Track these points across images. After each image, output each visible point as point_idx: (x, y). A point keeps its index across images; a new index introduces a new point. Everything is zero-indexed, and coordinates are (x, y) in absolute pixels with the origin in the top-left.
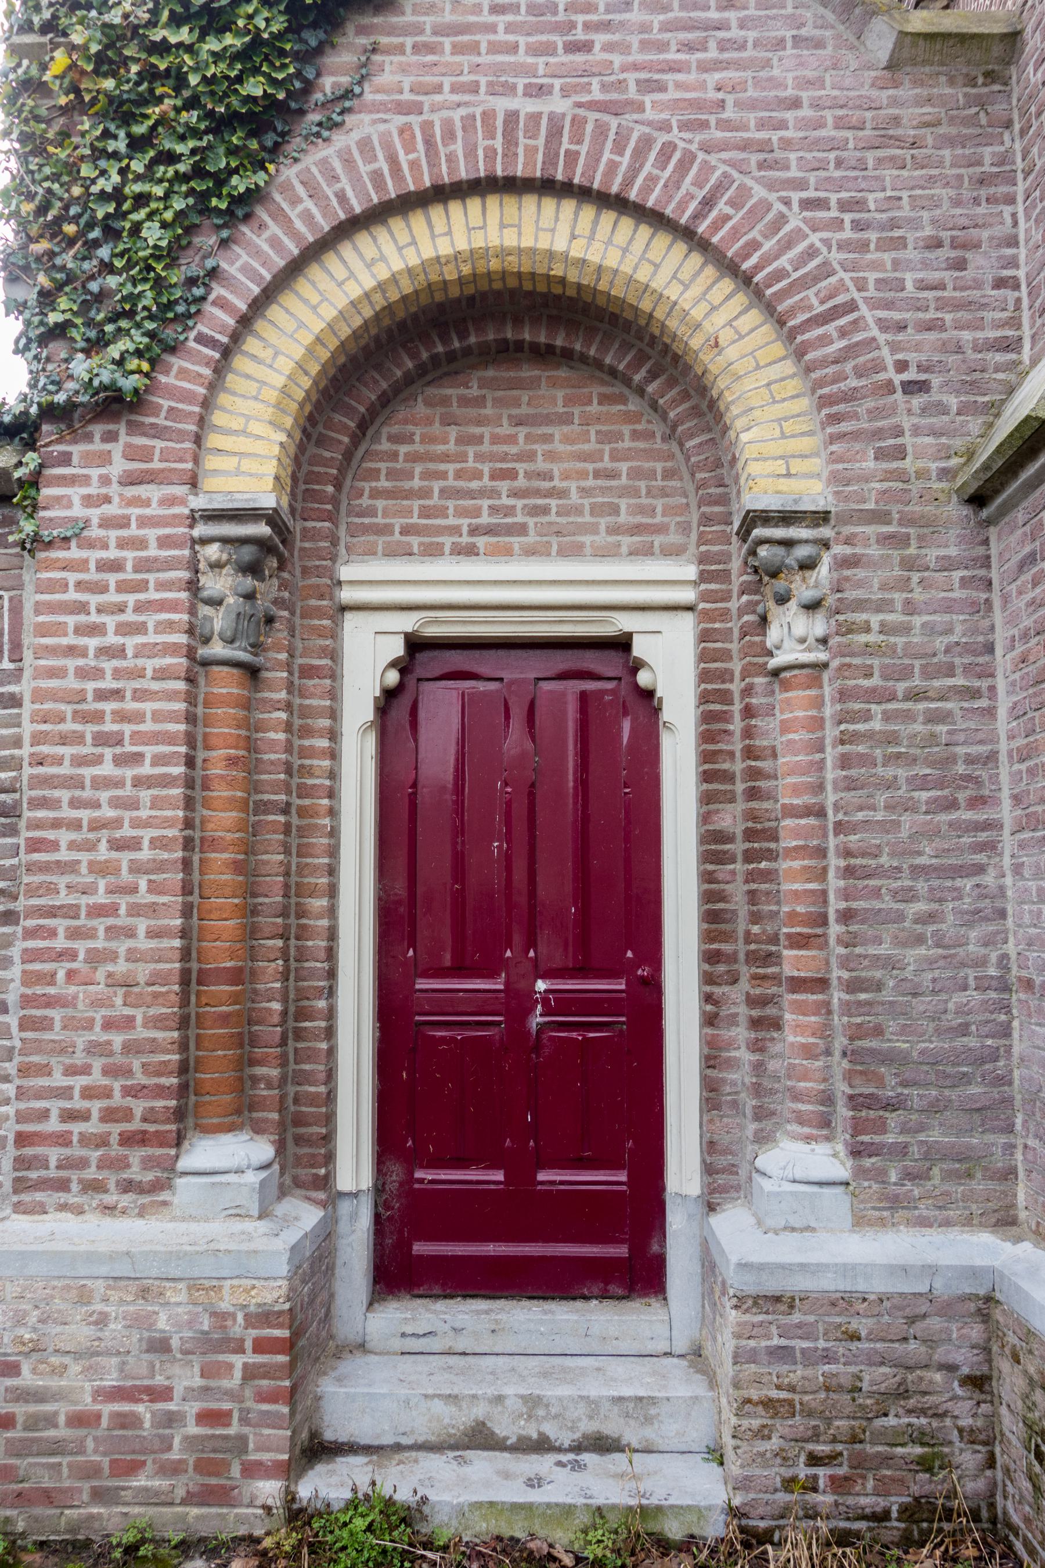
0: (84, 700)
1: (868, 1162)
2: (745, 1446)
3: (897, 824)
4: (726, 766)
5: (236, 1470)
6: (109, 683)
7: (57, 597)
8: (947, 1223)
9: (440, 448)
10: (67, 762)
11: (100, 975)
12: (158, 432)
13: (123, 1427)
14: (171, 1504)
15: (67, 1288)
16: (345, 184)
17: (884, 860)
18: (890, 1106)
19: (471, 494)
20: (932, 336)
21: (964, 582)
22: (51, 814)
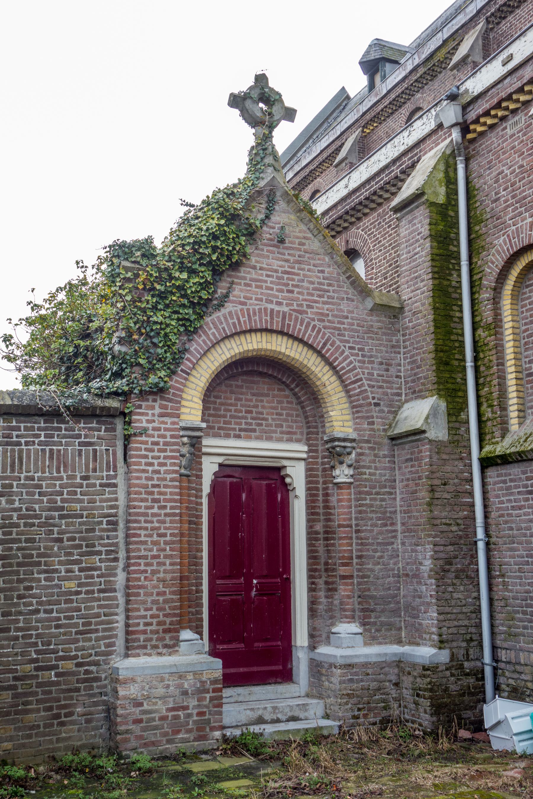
0: (148, 488)
1: (367, 627)
2: (342, 707)
3: (373, 530)
4: (318, 511)
5: (208, 729)
6: (155, 482)
7: (139, 453)
8: (386, 643)
9: (230, 401)
10: (143, 508)
11: (155, 578)
12: (170, 400)
13: (175, 719)
14: (189, 742)
15: (157, 677)
16: (224, 325)
17: (370, 540)
18: (372, 611)
19: (239, 418)
20: (380, 390)
21: (389, 461)
22: (138, 525)
